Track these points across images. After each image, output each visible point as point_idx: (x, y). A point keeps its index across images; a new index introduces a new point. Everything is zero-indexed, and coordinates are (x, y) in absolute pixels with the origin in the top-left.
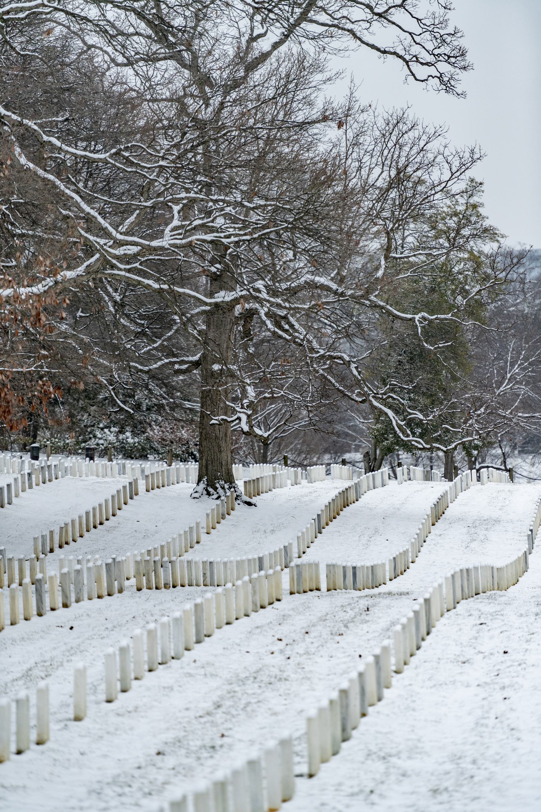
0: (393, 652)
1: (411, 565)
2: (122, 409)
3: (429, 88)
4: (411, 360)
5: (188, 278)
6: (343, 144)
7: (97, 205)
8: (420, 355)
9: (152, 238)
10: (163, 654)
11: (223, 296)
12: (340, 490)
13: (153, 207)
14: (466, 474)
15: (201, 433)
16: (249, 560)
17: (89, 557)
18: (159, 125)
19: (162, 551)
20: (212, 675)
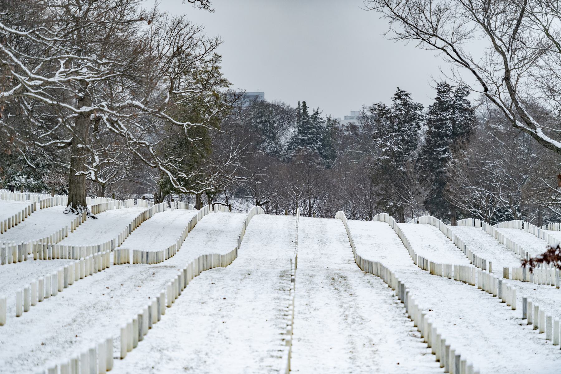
0: (166, 296)
1: (177, 252)
2: (29, 166)
3: (196, 6)
4: (181, 146)
5: (67, 99)
6: (150, 33)
7: (21, 59)
8: (186, 144)
9: (49, 77)
10: (47, 293)
11: (84, 109)
12: (142, 212)
13: (50, 61)
14: (207, 207)
15: (70, 180)
16: (93, 247)
17: (9, 242)
18: (55, 19)
19: (48, 240)
20: (72, 305)
